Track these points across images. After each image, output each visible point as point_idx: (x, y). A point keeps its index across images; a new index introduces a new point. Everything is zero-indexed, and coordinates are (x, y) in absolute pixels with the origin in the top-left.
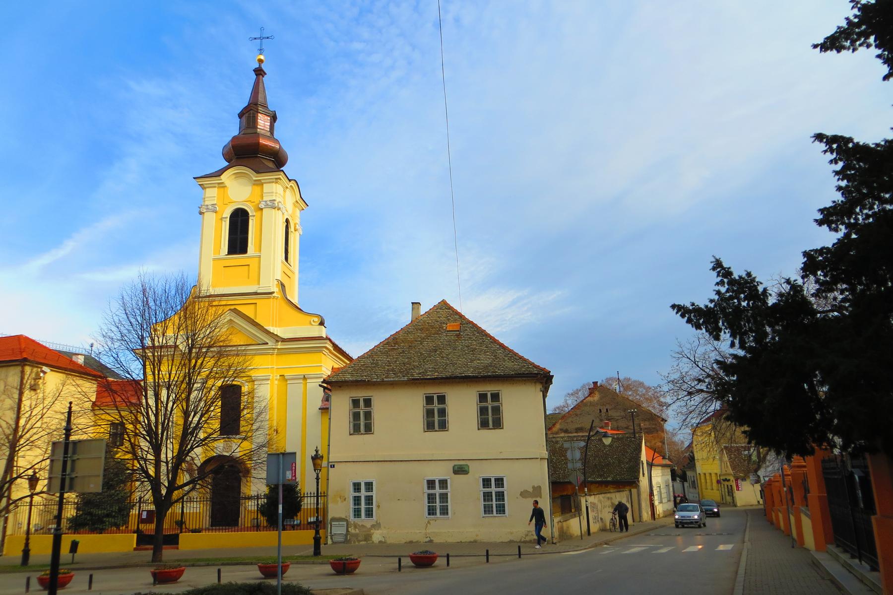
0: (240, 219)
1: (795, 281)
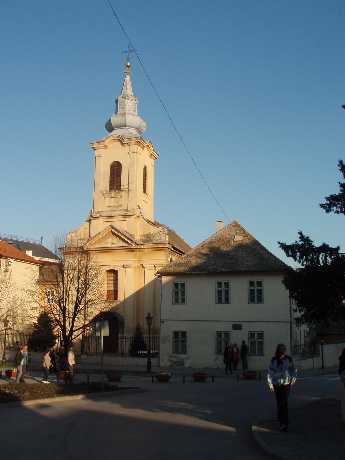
1: (178, 234)
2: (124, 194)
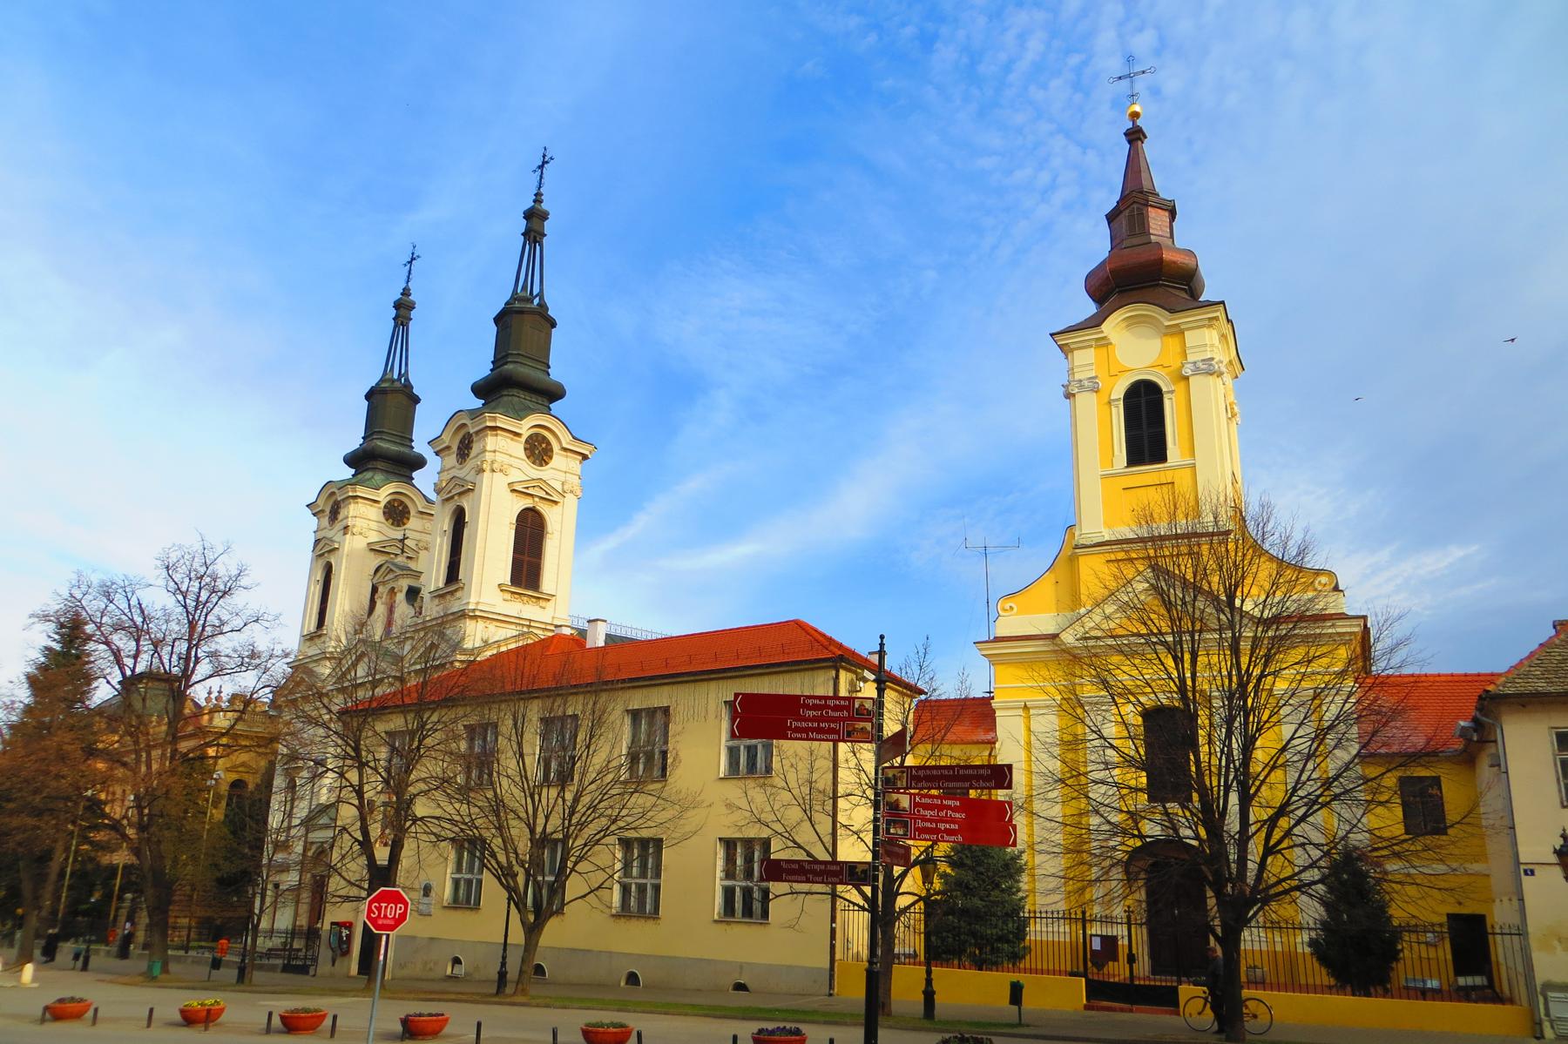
0: (1143, 400)
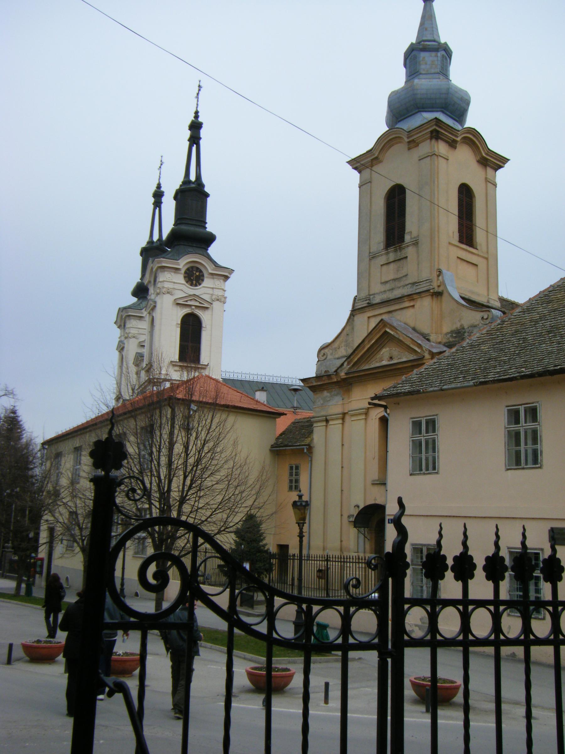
2: (410, 251)
